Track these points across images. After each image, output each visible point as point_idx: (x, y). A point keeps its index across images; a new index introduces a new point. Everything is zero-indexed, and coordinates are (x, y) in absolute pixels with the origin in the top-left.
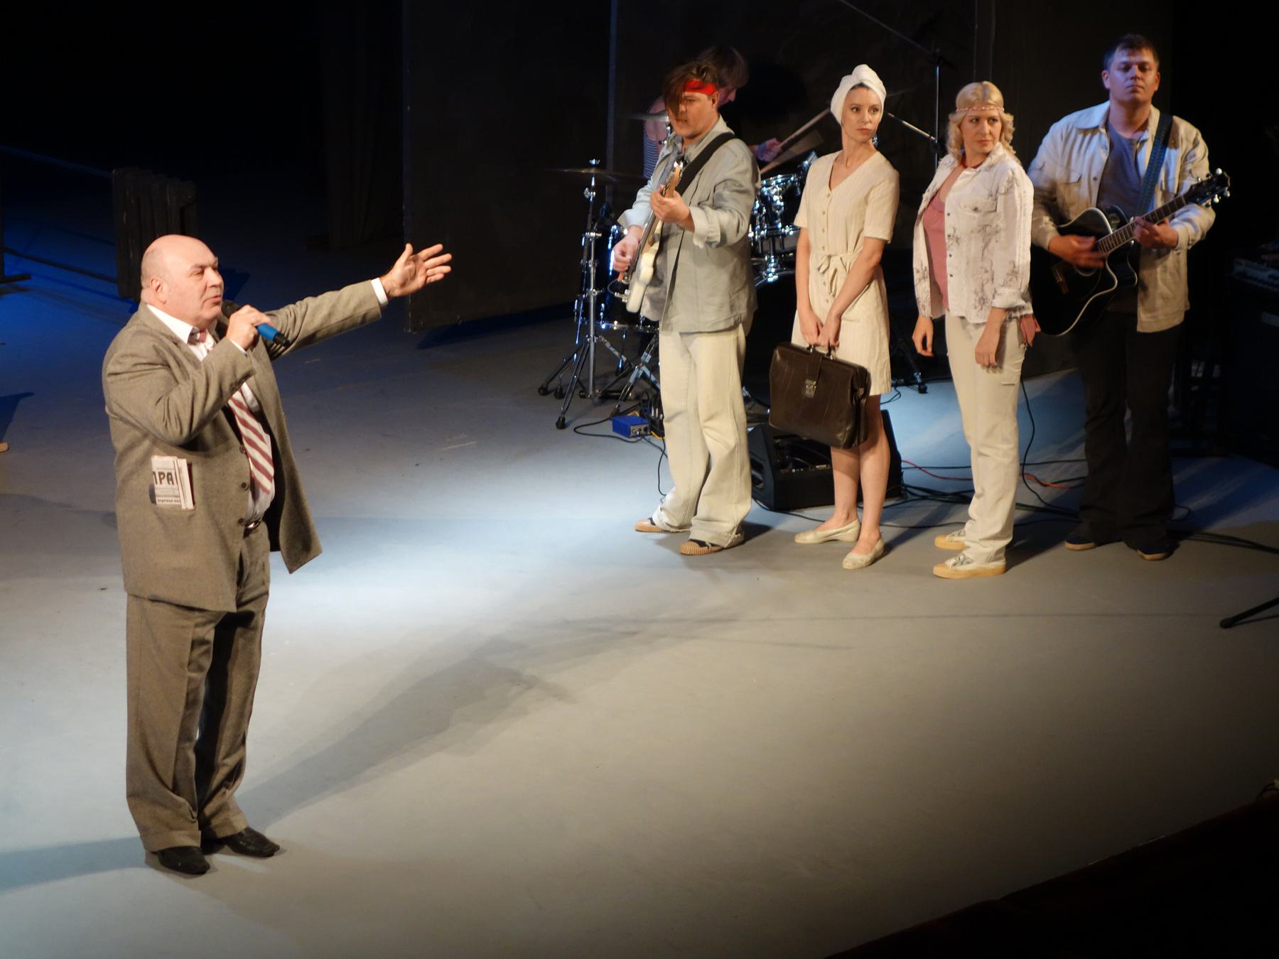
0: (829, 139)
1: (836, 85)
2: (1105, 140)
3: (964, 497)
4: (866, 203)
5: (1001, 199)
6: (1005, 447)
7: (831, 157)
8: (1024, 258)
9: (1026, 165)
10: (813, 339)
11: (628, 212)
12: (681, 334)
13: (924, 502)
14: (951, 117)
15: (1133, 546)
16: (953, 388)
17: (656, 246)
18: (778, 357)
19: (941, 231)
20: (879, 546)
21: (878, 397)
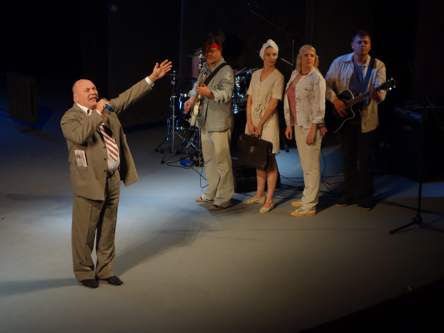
0: (259, 64)
1: (261, 47)
2: (352, 65)
3: (301, 188)
4: (273, 86)
5: (315, 86)
6: (316, 171)
7: (261, 70)
8: (323, 107)
9: (324, 74)
10: (253, 133)
11: (191, 92)
12: (209, 132)
13: (291, 189)
14: (298, 56)
15: (360, 205)
16: (298, 151)
17: (199, 103)
18: (241, 138)
19: (294, 96)
20: (272, 205)
21: (274, 155)
